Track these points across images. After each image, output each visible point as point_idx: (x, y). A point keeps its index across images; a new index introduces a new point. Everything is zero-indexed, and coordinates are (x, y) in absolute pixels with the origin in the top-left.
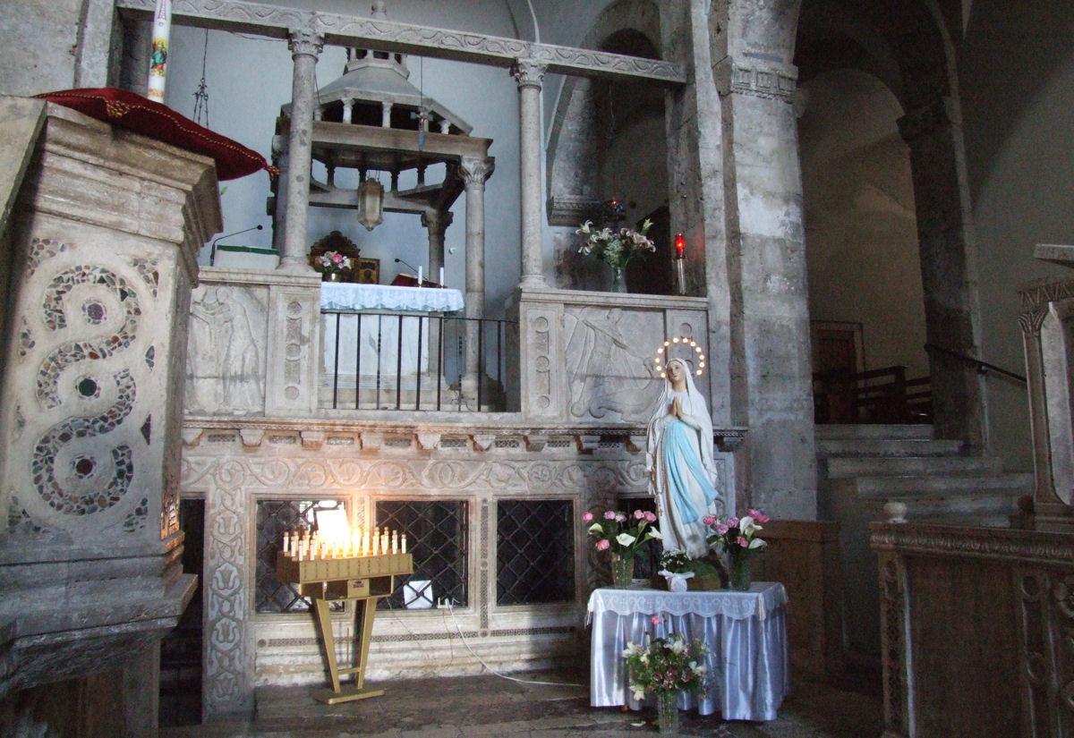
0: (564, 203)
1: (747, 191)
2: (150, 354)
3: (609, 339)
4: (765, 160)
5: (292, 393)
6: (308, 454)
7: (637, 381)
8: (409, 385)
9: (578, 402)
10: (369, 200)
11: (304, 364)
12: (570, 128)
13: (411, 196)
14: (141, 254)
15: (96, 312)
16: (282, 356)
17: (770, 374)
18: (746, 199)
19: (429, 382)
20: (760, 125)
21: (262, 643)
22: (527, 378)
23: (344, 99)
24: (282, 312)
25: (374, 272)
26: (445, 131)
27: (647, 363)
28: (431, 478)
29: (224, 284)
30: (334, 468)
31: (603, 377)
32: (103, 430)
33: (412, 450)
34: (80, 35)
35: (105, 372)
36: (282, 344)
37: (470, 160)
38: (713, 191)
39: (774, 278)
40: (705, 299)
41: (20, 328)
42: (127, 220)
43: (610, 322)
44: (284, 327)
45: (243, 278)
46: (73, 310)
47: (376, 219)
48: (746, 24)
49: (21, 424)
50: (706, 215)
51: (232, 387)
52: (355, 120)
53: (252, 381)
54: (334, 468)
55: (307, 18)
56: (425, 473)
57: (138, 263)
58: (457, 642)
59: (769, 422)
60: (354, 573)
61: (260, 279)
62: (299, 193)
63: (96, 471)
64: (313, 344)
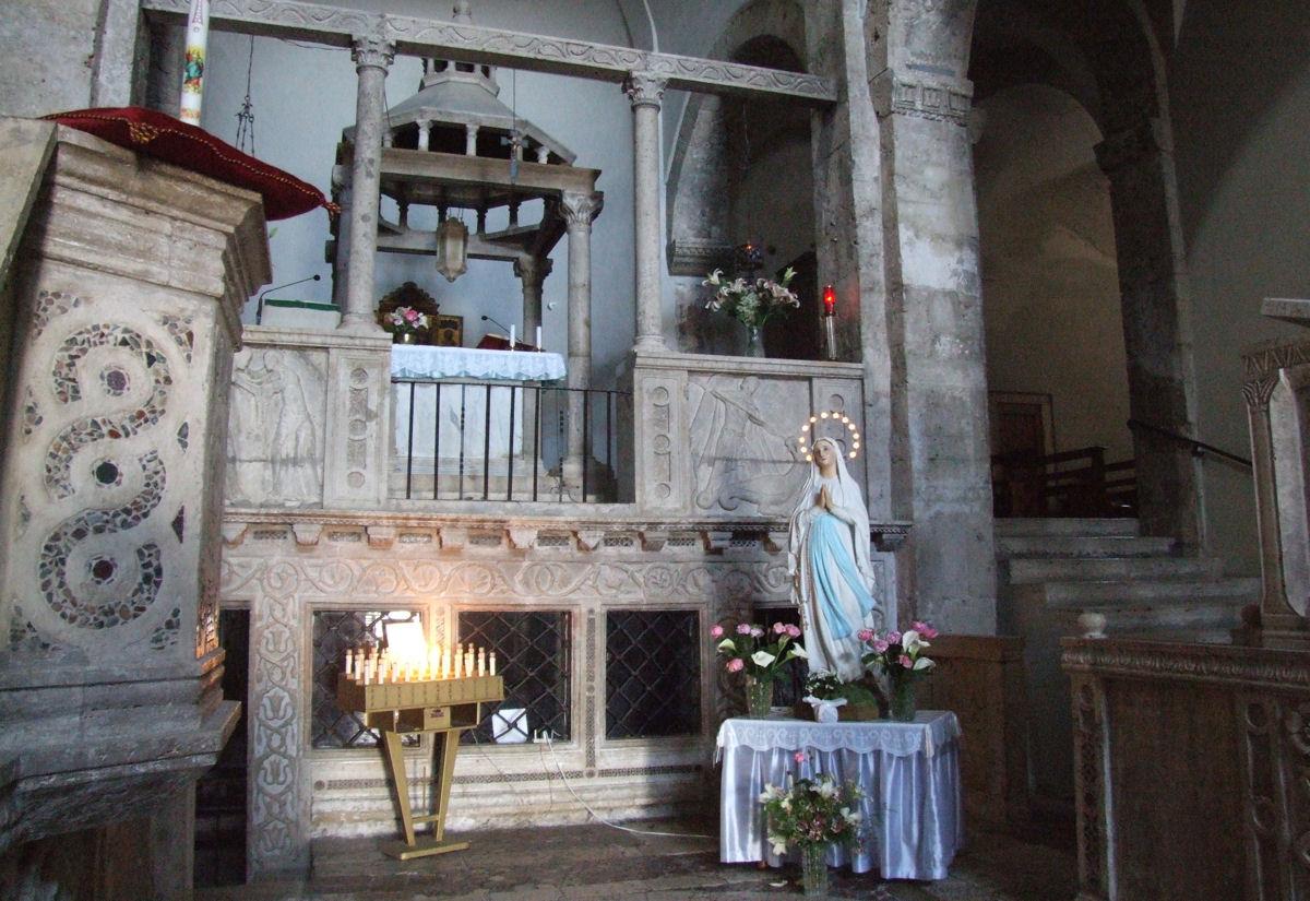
0: (688, 248)
1: (911, 233)
2: (183, 433)
3: (743, 414)
4: (933, 195)
5: (356, 479)
6: (376, 555)
7: (777, 465)
8: (499, 469)
9: (705, 491)
10: (450, 245)
11: (371, 445)
12: (695, 156)
13: (501, 239)
14: (172, 310)
15: (117, 381)
16: (344, 434)
17: (940, 457)
18: (910, 243)
19: (523, 466)
20: (926, 152)
21: (319, 785)
22: (642, 461)
23: (419, 121)
24: (344, 381)
25: (457, 333)
26: (543, 159)
27: (789, 443)
28: (526, 583)
29: (274, 346)
30: (408, 572)
31: (736, 460)
32: (125, 525)
33: (502, 549)
34: (98, 43)
35: (128, 454)
36: (345, 420)
37: (573, 196)
38: (869, 233)
39: (944, 339)
40: (860, 366)
41: (24, 401)
42: (155, 269)
43: (744, 393)
44: (346, 399)
45: (296, 340)
46: (89, 379)
47: (459, 267)
48: (910, 29)
49: (26, 517)
50: (861, 263)
51: (283, 472)
52: (433, 146)
53: (307, 465)
54: (408, 572)
55: (374, 21)
56: (519, 577)
57: (168, 321)
58: (557, 784)
59: (938, 515)
60: (432, 699)
61: (318, 341)
62: (364, 235)
63: (117, 575)
64: (382, 421)
